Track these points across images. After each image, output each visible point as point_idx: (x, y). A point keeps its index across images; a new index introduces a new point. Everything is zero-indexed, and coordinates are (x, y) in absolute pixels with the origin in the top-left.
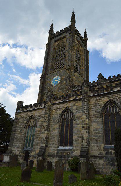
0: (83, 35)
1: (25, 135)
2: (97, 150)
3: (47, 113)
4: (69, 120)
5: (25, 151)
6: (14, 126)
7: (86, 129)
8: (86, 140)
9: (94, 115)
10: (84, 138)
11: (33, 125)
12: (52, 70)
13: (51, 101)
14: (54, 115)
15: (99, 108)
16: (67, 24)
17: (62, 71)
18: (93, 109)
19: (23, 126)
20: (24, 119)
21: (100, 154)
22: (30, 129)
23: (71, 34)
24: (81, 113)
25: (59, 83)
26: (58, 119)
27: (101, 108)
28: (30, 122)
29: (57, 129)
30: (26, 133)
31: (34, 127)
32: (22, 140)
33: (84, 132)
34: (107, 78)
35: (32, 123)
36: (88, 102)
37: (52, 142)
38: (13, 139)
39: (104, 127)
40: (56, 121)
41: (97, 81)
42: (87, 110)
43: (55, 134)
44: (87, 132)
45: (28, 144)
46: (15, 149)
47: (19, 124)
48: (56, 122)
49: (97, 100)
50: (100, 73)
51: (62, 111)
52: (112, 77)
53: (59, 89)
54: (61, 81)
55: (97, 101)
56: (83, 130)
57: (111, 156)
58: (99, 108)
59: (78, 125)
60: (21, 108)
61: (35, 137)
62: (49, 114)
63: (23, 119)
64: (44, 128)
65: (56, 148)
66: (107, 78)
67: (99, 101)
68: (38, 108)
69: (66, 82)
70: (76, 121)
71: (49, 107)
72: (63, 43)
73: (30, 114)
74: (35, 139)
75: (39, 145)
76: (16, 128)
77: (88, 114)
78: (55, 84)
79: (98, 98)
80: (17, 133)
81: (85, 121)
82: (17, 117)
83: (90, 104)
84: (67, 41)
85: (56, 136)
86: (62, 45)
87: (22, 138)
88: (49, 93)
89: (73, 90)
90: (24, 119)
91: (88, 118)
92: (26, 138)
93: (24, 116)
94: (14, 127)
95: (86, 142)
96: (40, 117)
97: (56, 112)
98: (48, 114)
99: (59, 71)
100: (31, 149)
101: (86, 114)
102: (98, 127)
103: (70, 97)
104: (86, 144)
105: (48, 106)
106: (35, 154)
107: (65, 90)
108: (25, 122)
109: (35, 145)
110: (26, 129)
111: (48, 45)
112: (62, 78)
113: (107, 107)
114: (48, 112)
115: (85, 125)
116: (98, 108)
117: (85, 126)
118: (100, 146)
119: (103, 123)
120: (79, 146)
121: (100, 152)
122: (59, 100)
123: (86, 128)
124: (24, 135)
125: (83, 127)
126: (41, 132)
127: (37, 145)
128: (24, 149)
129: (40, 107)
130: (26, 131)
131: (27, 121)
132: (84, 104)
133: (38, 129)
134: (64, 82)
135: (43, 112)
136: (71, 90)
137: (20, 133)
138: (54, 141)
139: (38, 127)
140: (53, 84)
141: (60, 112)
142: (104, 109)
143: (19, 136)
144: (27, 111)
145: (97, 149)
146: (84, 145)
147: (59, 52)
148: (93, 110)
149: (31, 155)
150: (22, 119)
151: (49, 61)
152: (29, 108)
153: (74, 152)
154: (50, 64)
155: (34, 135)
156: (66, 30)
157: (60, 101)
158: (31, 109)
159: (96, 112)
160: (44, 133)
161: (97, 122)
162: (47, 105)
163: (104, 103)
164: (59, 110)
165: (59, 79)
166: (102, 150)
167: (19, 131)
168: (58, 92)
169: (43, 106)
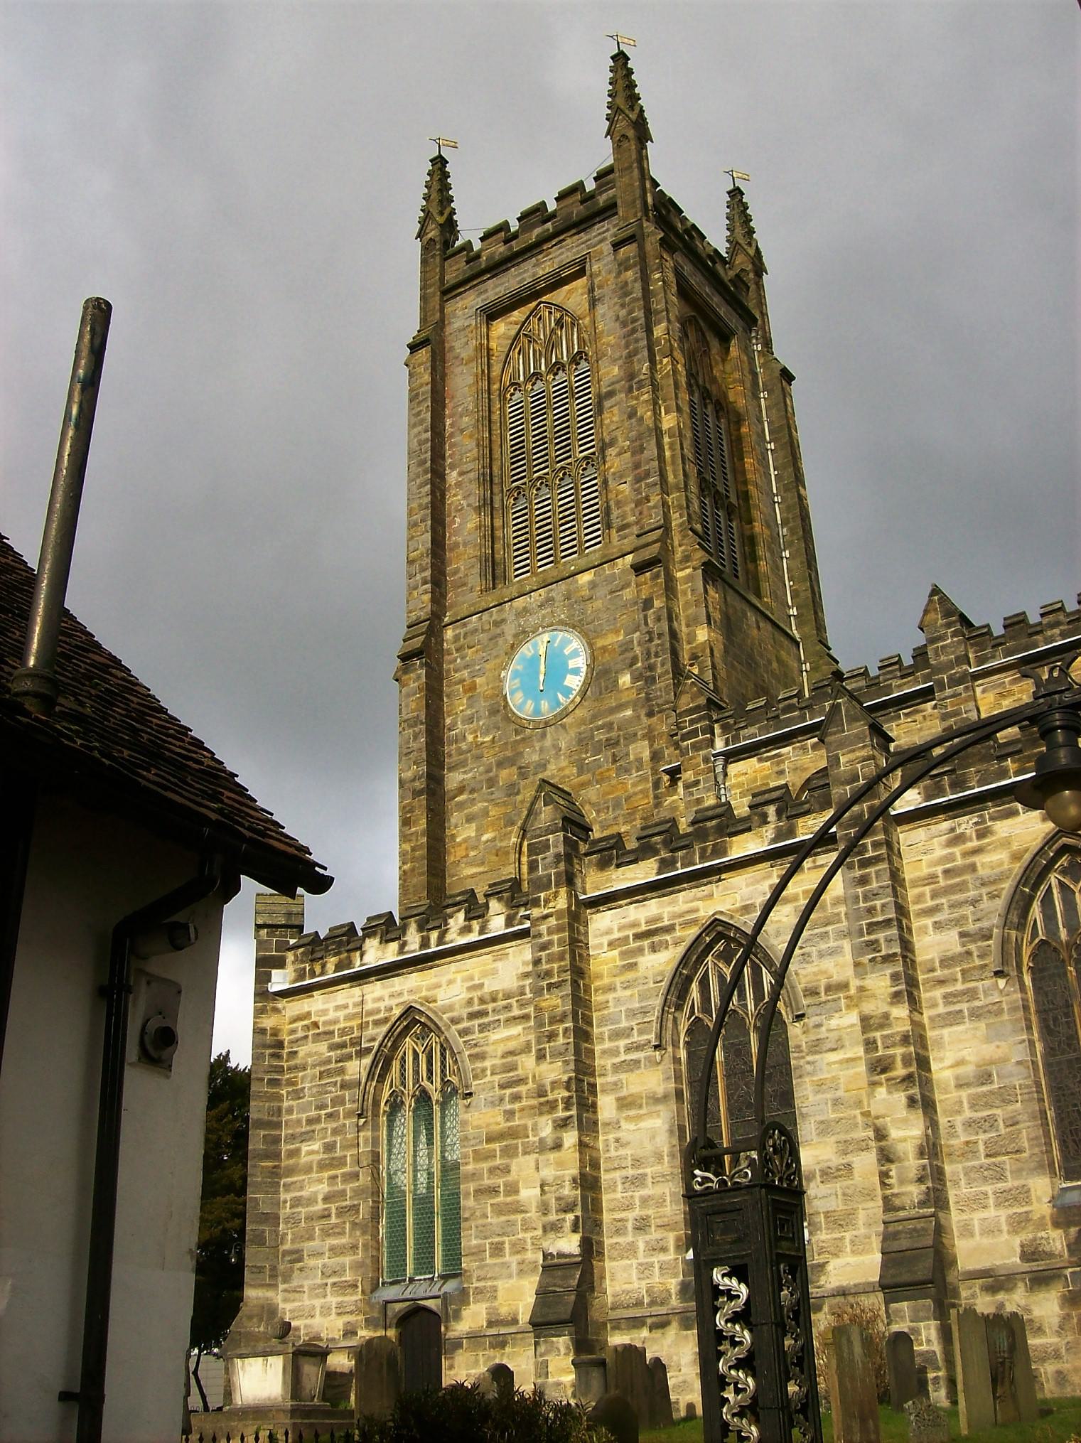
0: (717, 238)
1: (376, 1177)
2: (1005, 1228)
3: (558, 985)
4: (751, 1021)
5: (398, 1306)
6: (257, 1110)
7: (908, 1078)
8: (913, 1164)
9: (946, 962)
10: (900, 1148)
11: (434, 1090)
12: (494, 572)
13: (569, 880)
14: (611, 988)
15: (986, 904)
16: (587, 155)
17: (593, 585)
18: (938, 917)
19: (338, 1101)
20: (343, 1046)
21: (1030, 1253)
22: (406, 1118)
23: (629, 251)
24: (848, 957)
25: (583, 693)
26: (654, 1017)
27: (1000, 904)
28: (396, 1064)
29: (656, 1100)
30: (376, 1158)
31: (443, 1111)
32: (354, 1224)
33: (890, 1103)
34: (998, 630)
35: (407, 1074)
36: (890, 862)
37: (629, 1207)
38: (273, 1219)
39: (1039, 1047)
40: (636, 1038)
41: (920, 654)
42: (894, 932)
43: (649, 1147)
44: (912, 1102)
45: (410, 1252)
46: (306, 1301)
47: (298, 1095)
48: (639, 1047)
49: (958, 839)
50: (936, 591)
51: (681, 950)
52: (1034, 618)
53: (584, 742)
54: (599, 677)
55: (957, 850)
56: (882, 1092)
57: (641, 988)
58: (986, 904)
59: (833, 1057)
60: (290, 956)
61: (472, 1187)
62: (575, 984)
63: (333, 1047)
64: (552, 1106)
65: (671, 1256)
66: (998, 630)
67: (975, 843)
68: (455, 938)
69: (646, 678)
70: (810, 1021)
71: (559, 929)
72: (565, 320)
73: (384, 997)
74: (468, 1203)
75: (513, 1245)
76: (278, 1125)
77: (904, 957)
78: (545, 705)
79: (966, 824)
80: (291, 1171)
81: (886, 1016)
82: (275, 1032)
83: (908, 874)
84: (601, 309)
85: (659, 1157)
86: (552, 345)
87: (354, 1209)
88: (546, 815)
89: (720, 745)
90: (343, 1046)
91: (909, 991)
92: (383, 1201)
93: (332, 1015)
94: (261, 1124)
95: (921, 1180)
96: (483, 1014)
97: (633, 966)
98: (568, 989)
99: (562, 586)
100: (450, 1286)
101: (888, 959)
102: (990, 1051)
103: (732, 835)
104: (915, 1192)
105: (553, 921)
106: (491, 1324)
107: (641, 749)
108: (357, 1068)
109: (479, 1251)
110: (376, 1128)
111: (430, 343)
112: (600, 643)
113: (1043, 888)
114: (562, 970)
115: (894, 1045)
116: (974, 902)
117: (893, 1057)
118: (1023, 1195)
119: (1028, 1020)
120: (861, 1215)
121: (1025, 1236)
122: (634, 861)
123: (900, 1071)
124: (365, 1179)
125: (880, 1067)
126: (509, 1139)
127: (497, 1250)
128: (391, 1293)
129: (466, 930)
130: (375, 1141)
131: (367, 1061)
132: (863, 881)
133: (481, 1115)
134: (625, 679)
135: (509, 968)
136: (696, 747)
137: (322, 1166)
138: (645, 1201)
139: (480, 1098)
140: (522, 705)
141: (660, 962)
142: (1019, 904)
143: (324, 1188)
144: (361, 978)
145: (1003, 1219)
146: (906, 1201)
147: (540, 412)
148: (938, 926)
149: (461, 1328)
150: (322, 1047)
151: (455, 498)
152: (372, 945)
153: (830, 1268)
154: (465, 525)
155: (456, 1166)
156: (578, 210)
157: (645, 872)
158: (390, 954)
159: (962, 935)
160: (558, 1146)
161: (976, 1014)
162: (546, 917)
163: (1016, 857)
164: (654, 949)
165: (575, 654)
166: (1041, 1225)
167: (311, 1150)
168: (580, 773)
169: (497, 925)
